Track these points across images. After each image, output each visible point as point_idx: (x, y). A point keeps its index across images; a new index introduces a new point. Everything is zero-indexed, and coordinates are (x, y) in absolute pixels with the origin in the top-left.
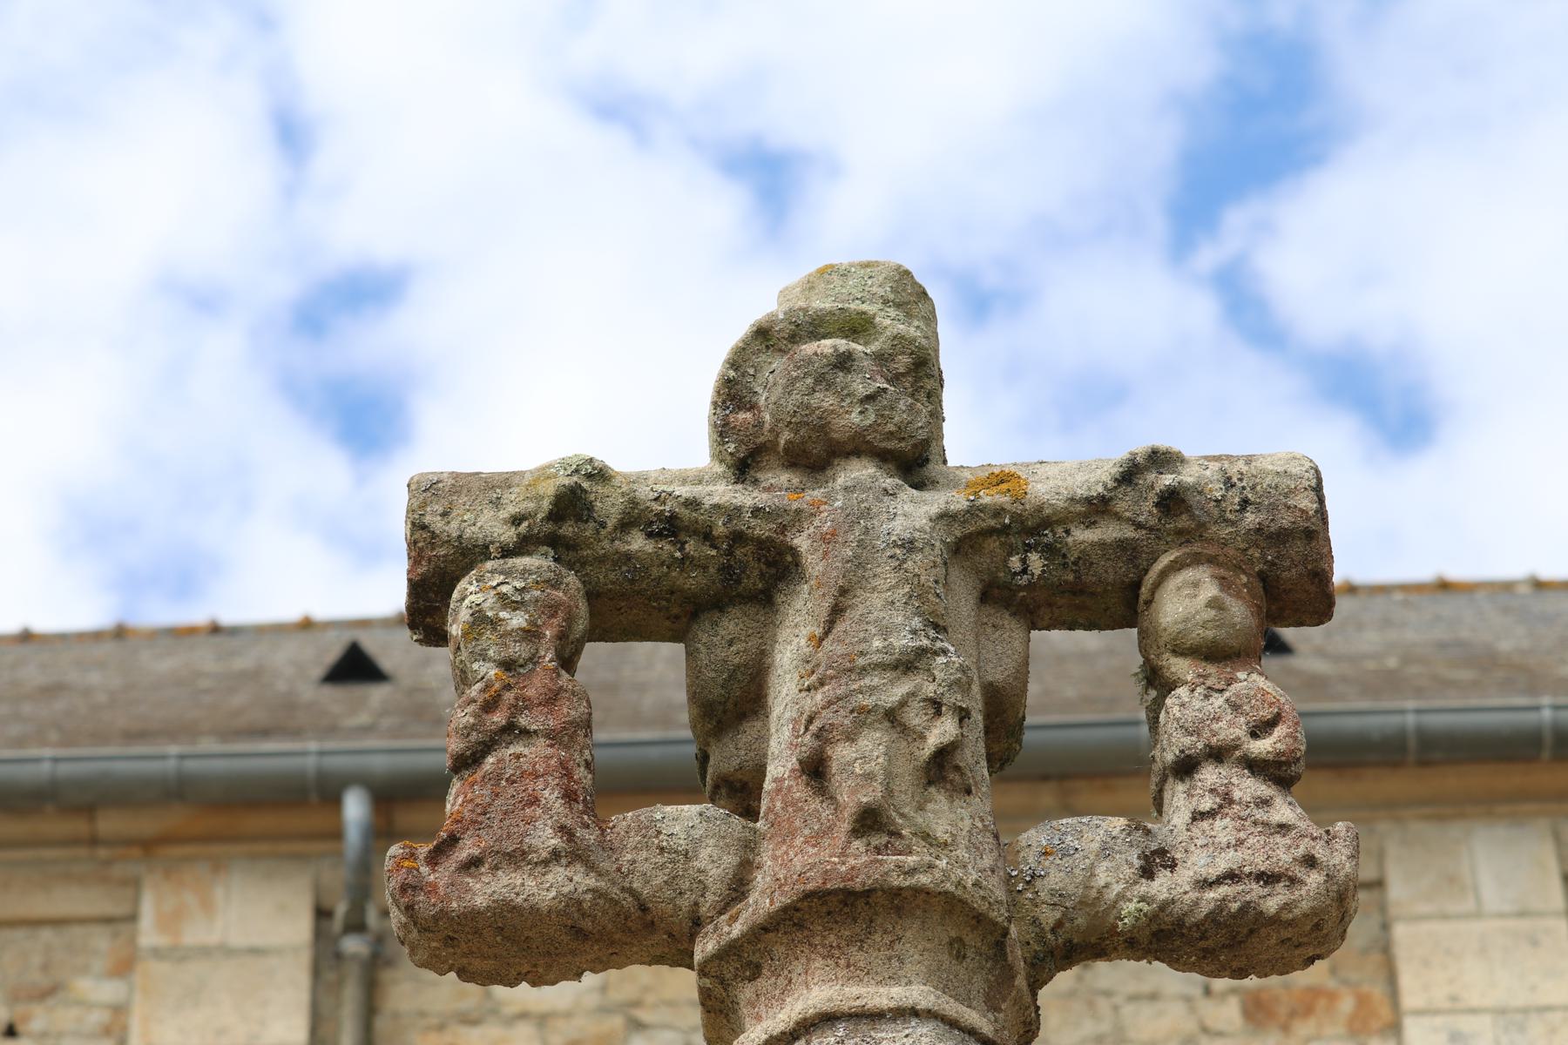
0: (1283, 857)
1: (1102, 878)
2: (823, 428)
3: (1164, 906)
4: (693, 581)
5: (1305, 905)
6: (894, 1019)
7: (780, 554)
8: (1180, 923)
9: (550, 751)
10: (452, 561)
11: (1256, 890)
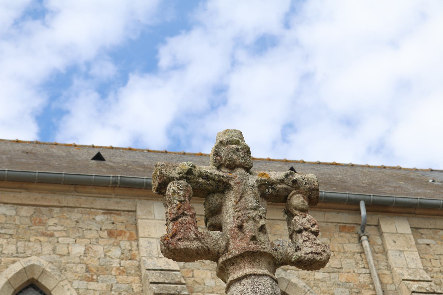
0: (320, 250)
1: (289, 251)
2: (234, 162)
3: (300, 257)
4: (210, 188)
5: (324, 259)
6: (262, 276)
7: (227, 185)
8: (302, 260)
9: (191, 219)
10: (167, 180)
11: (315, 256)
